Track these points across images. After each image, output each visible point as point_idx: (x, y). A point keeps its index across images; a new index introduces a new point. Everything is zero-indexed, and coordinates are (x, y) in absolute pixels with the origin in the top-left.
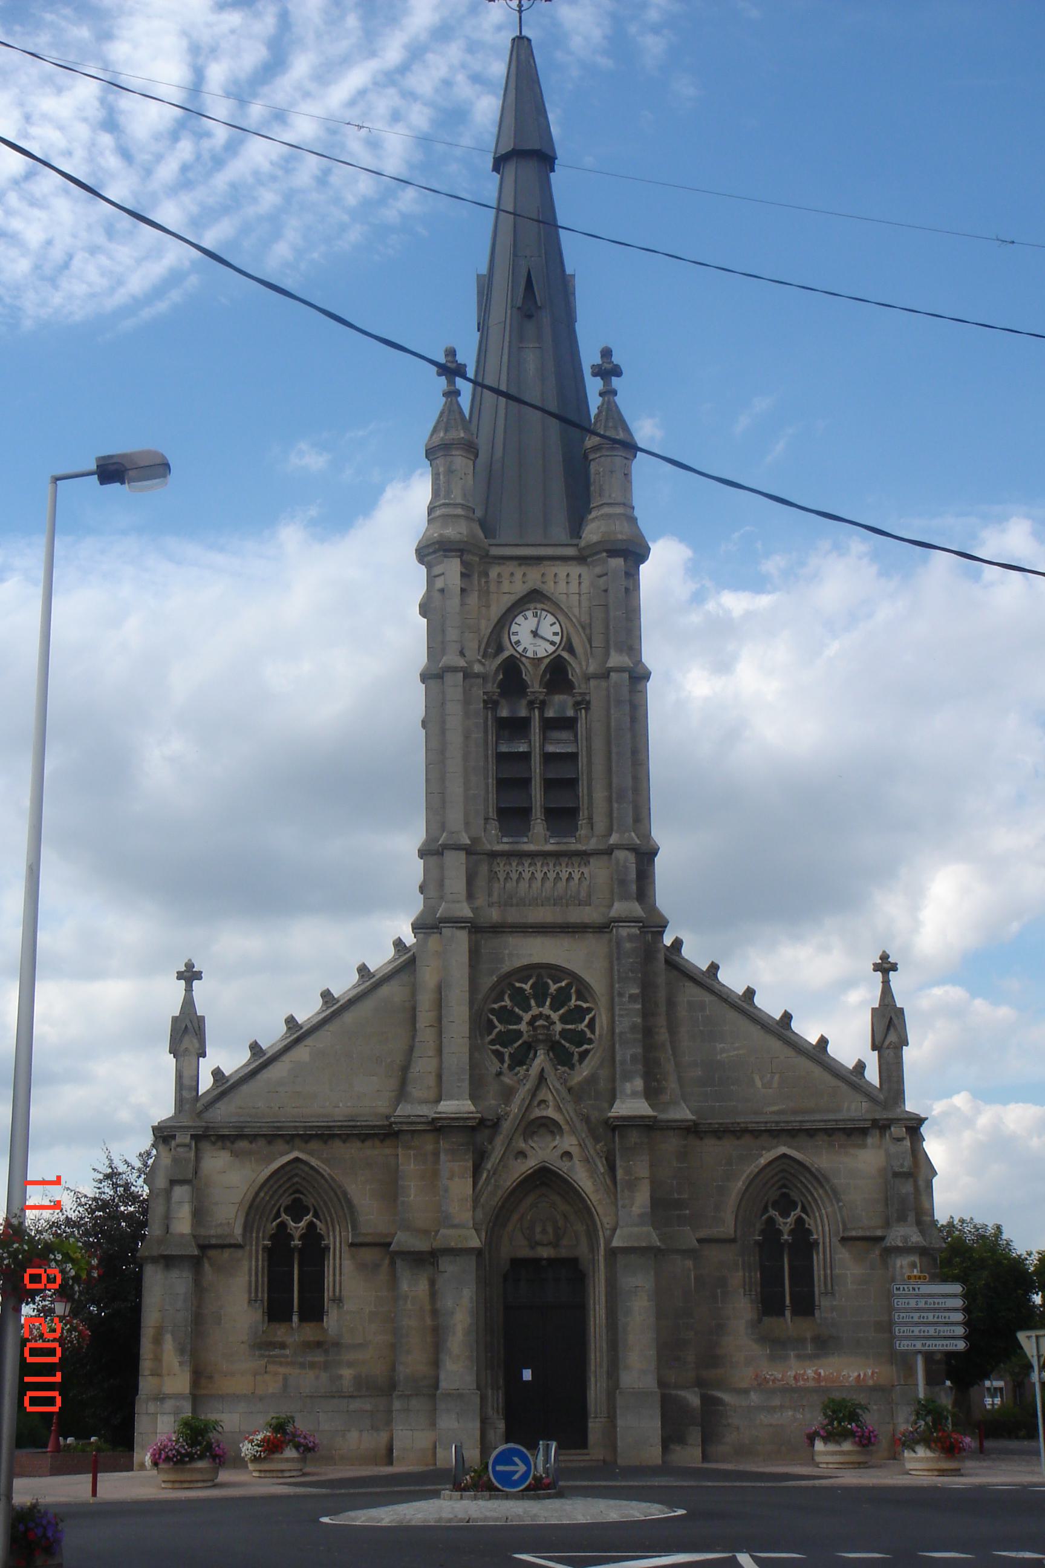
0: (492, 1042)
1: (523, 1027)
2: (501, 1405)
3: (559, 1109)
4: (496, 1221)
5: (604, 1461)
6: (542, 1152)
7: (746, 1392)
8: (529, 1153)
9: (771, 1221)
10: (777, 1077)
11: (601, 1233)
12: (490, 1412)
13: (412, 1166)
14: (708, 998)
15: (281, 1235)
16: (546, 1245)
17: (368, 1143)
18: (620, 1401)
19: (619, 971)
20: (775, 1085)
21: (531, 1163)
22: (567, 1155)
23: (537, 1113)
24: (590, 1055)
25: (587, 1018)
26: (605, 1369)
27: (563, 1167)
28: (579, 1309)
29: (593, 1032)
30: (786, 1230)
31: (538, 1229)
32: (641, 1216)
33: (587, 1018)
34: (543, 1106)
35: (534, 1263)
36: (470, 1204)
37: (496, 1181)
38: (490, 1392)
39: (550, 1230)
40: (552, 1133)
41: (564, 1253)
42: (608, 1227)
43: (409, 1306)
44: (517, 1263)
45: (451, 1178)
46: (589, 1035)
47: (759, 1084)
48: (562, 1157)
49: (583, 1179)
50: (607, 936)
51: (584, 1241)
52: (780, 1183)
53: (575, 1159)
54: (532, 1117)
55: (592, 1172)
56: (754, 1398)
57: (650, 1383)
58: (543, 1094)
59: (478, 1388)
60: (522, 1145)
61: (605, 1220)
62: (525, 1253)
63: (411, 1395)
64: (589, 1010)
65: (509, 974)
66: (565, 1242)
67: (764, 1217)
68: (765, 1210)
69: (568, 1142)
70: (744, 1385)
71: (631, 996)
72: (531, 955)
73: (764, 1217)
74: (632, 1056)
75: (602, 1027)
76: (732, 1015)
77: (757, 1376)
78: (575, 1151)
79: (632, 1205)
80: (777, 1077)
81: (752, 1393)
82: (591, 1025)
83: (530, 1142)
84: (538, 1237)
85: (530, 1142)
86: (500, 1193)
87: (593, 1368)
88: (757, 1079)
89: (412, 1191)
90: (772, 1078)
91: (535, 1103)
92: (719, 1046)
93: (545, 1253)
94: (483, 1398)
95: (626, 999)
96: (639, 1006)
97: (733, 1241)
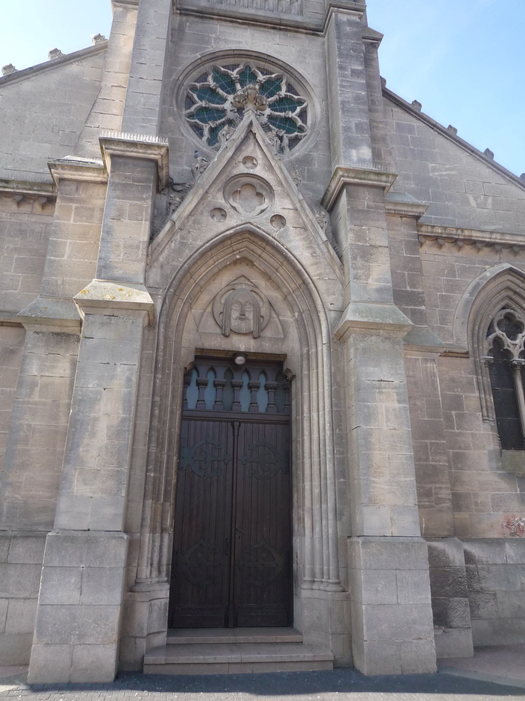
0: (191, 116)
1: (227, 106)
2: (165, 561)
3: (271, 168)
4: (177, 288)
5: (335, 662)
6: (245, 213)
7: (499, 542)
8: (230, 212)
9: (498, 341)
10: (490, 200)
11: (322, 315)
12: (145, 572)
13: (72, 222)
14: (416, 123)
15: (498, 348)
16: (245, 334)
17: (26, 208)
18: (362, 556)
19: (339, 48)
20: (490, 206)
21: (232, 222)
22: (279, 219)
23: (242, 169)
24: (302, 141)
25: (299, 109)
26: (331, 504)
27: (272, 231)
28: (284, 424)
29: (305, 121)
30: (516, 352)
31: (235, 314)
32: (380, 290)
33: (299, 109)
34: (249, 164)
35: (227, 359)
36: (141, 253)
37: (182, 238)
38: (147, 536)
39: (250, 316)
40: (259, 195)
41: (267, 347)
42: (331, 307)
43: (36, 397)
44: (204, 358)
45: (118, 218)
46: (300, 123)
47: (473, 203)
48: (272, 221)
49: (298, 246)
50: (320, 39)
51: (294, 333)
52: (503, 304)
53: (289, 225)
54: (236, 172)
55: (310, 243)
56: (511, 552)
57: (408, 525)
58: (250, 150)
59: (126, 530)
60: (220, 201)
61: (328, 299)
62: (216, 343)
63: (15, 537)
64: (300, 102)
65: (214, 57)
66: (268, 333)
67: (491, 337)
68: (490, 330)
69: (281, 205)
70: (494, 535)
71: (353, 71)
72: (239, 42)
73: (491, 337)
74: (356, 125)
75: (315, 116)
76: (440, 140)
77: (508, 523)
78: (288, 215)
79: (368, 277)
80: (490, 200)
81: (507, 545)
82: (303, 115)
83: (231, 201)
84: (235, 324)
85: (231, 201)
86: (187, 253)
87: (307, 503)
88: (471, 198)
89: (68, 250)
90: (486, 200)
91: (240, 158)
92: (431, 165)
93: (242, 344)
94: (133, 548)
95: (348, 73)
96: (364, 81)
97: (466, 355)
